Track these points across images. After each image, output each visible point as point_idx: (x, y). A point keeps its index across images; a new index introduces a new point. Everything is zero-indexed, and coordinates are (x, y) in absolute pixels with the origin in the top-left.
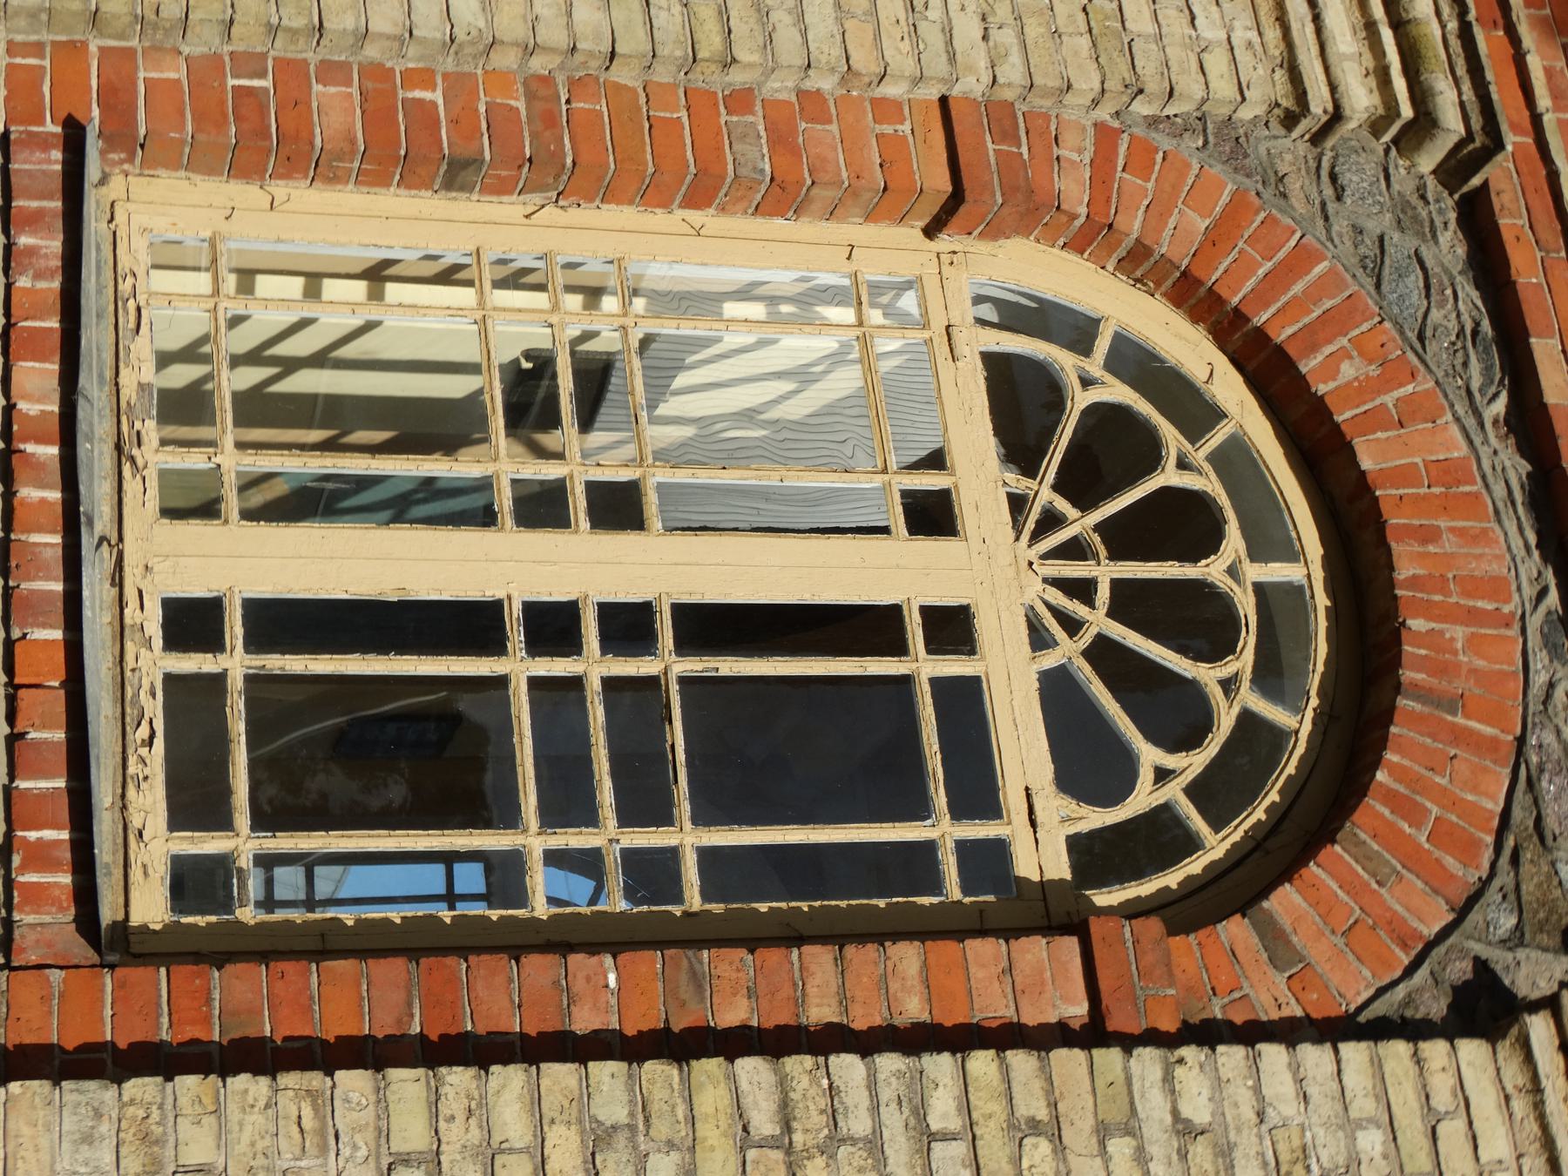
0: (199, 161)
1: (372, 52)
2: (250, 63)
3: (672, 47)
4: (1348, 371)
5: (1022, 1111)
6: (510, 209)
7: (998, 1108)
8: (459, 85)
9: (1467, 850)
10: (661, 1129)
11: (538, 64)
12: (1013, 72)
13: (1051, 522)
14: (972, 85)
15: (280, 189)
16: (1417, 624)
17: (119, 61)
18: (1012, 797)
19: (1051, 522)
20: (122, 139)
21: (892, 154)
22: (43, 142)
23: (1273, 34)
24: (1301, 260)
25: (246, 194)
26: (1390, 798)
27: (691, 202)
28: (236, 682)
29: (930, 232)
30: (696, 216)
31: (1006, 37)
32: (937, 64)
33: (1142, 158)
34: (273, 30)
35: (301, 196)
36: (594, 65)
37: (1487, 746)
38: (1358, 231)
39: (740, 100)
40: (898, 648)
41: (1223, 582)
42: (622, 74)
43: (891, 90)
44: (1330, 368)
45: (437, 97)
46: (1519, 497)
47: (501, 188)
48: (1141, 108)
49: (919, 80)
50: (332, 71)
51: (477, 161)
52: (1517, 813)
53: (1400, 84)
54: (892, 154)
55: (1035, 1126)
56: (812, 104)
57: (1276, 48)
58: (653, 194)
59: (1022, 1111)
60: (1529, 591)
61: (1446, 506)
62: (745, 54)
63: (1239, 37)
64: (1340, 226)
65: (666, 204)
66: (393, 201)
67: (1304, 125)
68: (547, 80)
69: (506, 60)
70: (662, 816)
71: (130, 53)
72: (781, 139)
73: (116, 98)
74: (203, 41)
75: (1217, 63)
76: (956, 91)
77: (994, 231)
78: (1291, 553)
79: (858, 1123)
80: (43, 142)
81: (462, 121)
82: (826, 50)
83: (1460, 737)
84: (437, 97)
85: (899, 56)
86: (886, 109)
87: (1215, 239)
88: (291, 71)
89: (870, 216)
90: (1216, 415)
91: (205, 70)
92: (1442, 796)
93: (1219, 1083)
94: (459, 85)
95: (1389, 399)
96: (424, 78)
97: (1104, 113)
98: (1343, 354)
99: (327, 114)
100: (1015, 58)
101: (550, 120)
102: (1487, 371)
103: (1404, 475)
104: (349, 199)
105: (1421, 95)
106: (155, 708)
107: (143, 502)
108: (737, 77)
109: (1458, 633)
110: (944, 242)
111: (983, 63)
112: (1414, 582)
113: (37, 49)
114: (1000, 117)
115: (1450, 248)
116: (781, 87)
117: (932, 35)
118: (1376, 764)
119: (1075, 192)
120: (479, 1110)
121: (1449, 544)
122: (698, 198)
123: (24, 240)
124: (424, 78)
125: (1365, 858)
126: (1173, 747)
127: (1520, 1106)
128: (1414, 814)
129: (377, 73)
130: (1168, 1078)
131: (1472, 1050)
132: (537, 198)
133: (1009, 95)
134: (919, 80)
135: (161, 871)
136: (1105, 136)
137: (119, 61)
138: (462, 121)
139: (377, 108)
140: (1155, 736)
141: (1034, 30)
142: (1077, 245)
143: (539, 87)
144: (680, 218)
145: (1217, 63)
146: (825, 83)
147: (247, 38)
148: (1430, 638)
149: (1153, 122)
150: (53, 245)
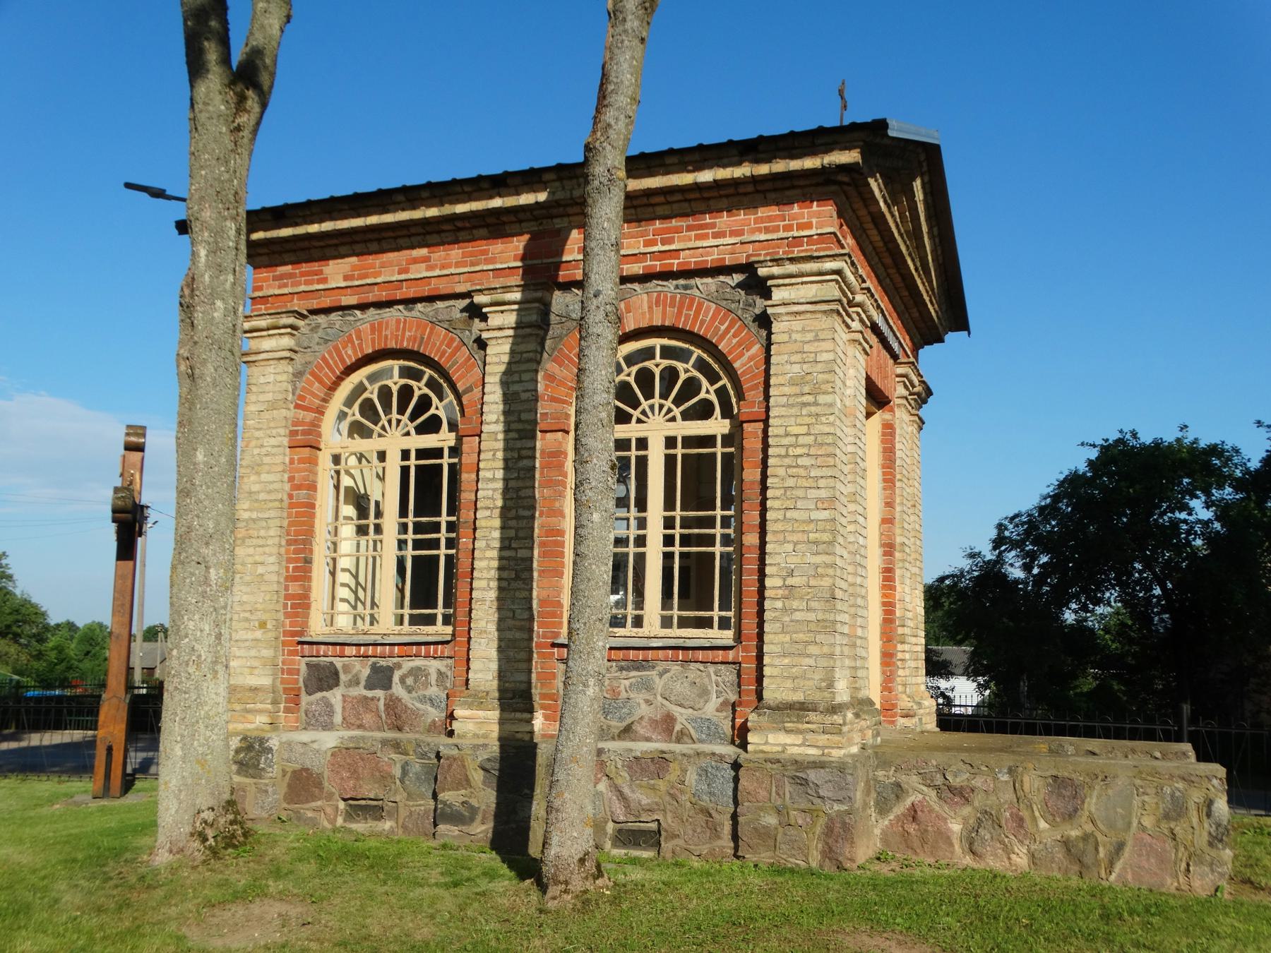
0: (307, 616)
1: (282, 580)
2: (285, 606)
3: (278, 513)
4: (350, 352)
5: (491, 457)
6: (316, 548)
7: (490, 463)
8: (289, 561)
9: (452, 340)
10: (487, 534)
11: (284, 543)
12: (282, 431)
13: (383, 428)
14: (286, 441)
15: (312, 599)
16: (405, 344)
17: (286, 633)
18: (439, 445)
19: (383, 428)
20: (301, 633)
21: (301, 461)
22: (302, 649)
23: (272, 362)
24: (324, 359)
25: (314, 606)
26: (441, 357)
27: (314, 508)
28: (410, 612)
29: (320, 450)
30: (317, 506)
31: (274, 432)
32: (281, 450)
33: (302, 398)
34: (278, 601)
35: (314, 595)
36: (284, 531)
37: (432, 329)
38: (318, 344)
39: (290, 496)
40: (408, 467)
41: (398, 386)
42: (285, 523)
43: (287, 460)
44: (349, 357)
45: (291, 566)
46: (379, 312)
47: (311, 551)
48: (290, 397)
49: (284, 454)
50: (287, 588)
51: (305, 558)
52: (445, 326)
53: (283, 331)
54: (301, 461)
55: (494, 455)
56: (291, 479)
57: (276, 362)
58: (313, 516)
59: (491, 457)
60: (399, 314)
61: (380, 332)
62: (279, 496)
63: (273, 371)
64: (317, 348)
65: (314, 514)
66: (315, 574)
67: (293, 357)
68: (287, 541)
69: (283, 550)
70: (439, 524)
71: (284, 631)
72: (299, 487)
73: (294, 634)
74: (281, 616)
75: (279, 378)
76: (287, 444)
77: (319, 435)
78: (391, 369)
79: (490, 493)
80: (302, 649)
81: (296, 560)
82: (277, 477)
83: (429, 338)
84: (291, 566)
85: (278, 459)
86: (292, 462)
87: (321, 382)
88: (287, 597)
89: (316, 464)
90: (361, 383)
91: (287, 615)
92: (441, 345)
93: (490, 412)
94: (289, 561)
95: (356, 342)
96: (287, 568)
97: (292, 406)
98: (346, 352)
99: (329, 532)
100: (279, 430)
101: (296, 541)
102: (350, 315)
103: (373, 341)
104: (314, 584)
105: (285, 327)
106: (414, 628)
107: (375, 629)
108: (285, 497)
109: (407, 334)
110: (322, 446)
111: (280, 439)
112: (396, 344)
113: (283, 650)
114: (293, 433)
115: (321, 319)
116: (287, 487)
117: (274, 451)
118: (433, 359)
119: (310, 416)
120: (481, 570)
121: (388, 333)
122: (313, 506)
123: (322, 653)
124: (287, 568)
125: (453, 365)
126: (431, 405)
127: (500, 341)
128: (444, 353)
129: (287, 579)
130: (488, 424)
131: (489, 350)
132: (314, 543)
133: (287, 431)
134: (284, 454)
135: (635, 630)
136: (297, 406)
137: (286, 633)
138: (296, 560)
139: (295, 579)
140: (428, 409)
141: (272, 425)
142: (322, 413)
143: (289, 543)
144: (318, 510)
145: (279, 378)
146: (286, 476)
147: (279, 607)
148: (408, 340)
149: (293, 394)
150: (323, 647)
